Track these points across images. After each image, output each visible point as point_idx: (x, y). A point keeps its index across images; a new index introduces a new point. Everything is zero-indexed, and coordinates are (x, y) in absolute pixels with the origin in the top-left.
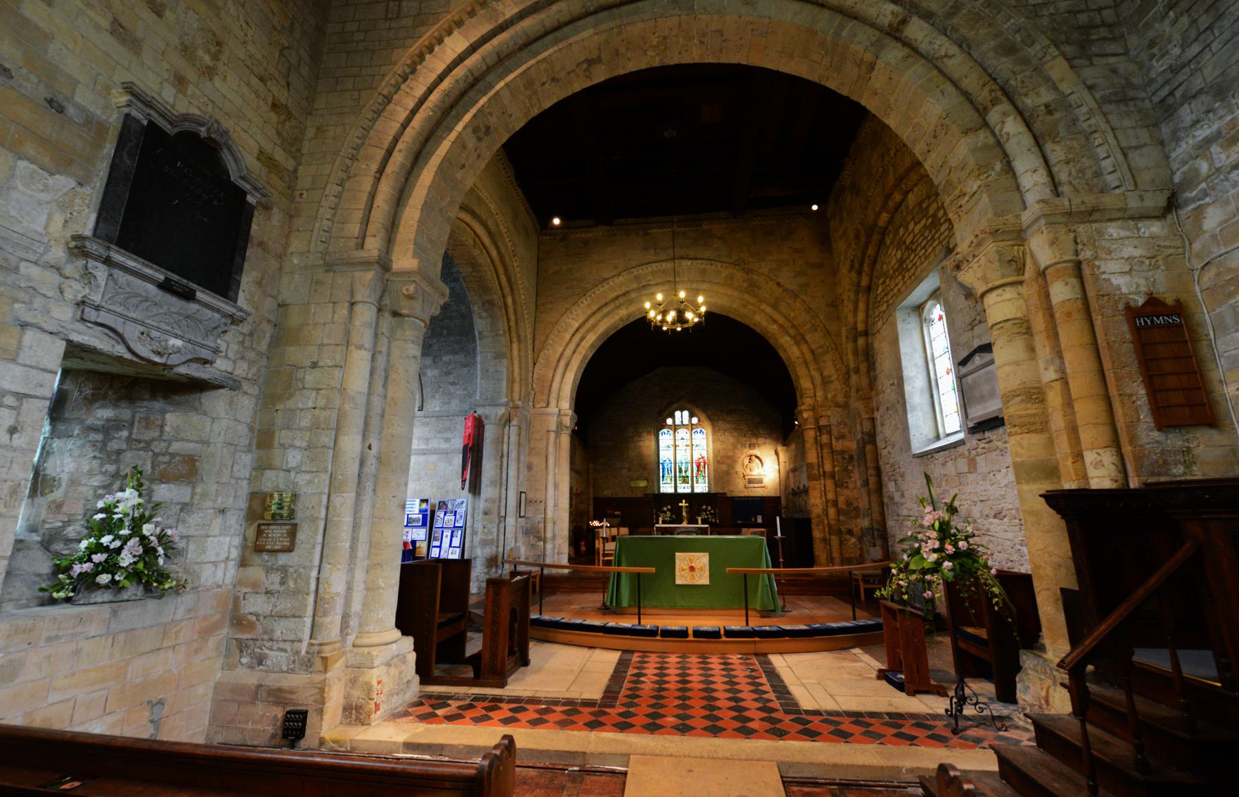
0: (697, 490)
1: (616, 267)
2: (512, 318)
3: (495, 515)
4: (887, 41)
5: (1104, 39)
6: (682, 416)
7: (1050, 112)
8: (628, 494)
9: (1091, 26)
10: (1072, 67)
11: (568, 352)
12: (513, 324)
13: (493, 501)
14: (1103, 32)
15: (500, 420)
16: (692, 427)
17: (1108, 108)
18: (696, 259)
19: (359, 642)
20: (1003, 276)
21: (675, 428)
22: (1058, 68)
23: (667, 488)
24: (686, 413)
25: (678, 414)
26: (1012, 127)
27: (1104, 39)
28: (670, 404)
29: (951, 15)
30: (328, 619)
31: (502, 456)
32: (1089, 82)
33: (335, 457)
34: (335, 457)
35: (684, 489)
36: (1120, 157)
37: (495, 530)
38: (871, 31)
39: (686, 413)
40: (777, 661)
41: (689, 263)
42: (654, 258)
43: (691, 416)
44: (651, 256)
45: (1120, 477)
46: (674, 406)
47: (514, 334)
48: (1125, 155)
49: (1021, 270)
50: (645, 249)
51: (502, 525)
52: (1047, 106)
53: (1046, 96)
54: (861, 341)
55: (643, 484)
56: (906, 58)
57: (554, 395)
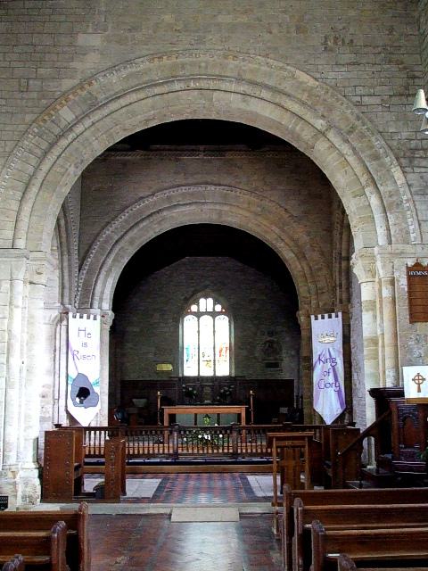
0: (218, 374)
1: (150, 188)
2: (64, 235)
3: (50, 399)
4: (320, 136)
5: (421, 157)
6: (206, 304)
7: (390, 196)
8: (155, 378)
9: (414, 150)
10: (404, 172)
11: (110, 261)
12: (64, 240)
13: (48, 386)
14: (421, 152)
15: (53, 321)
16: (214, 314)
17: (416, 198)
18: (220, 185)
19: (24, 466)
20: (367, 277)
21: (198, 315)
22: (397, 173)
23: (190, 370)
24: (210, 301)
25: (202, 301)
26: (374, 201)
27: (421, 157)
28: (194, 293)
29: (350, 132)
30: (11, 454)
31: (55, 351)
32: (409, 183)
33: (8, 369)
34: (8, 369)
35: (207, 372)
36: (417, 225)
37: (51, 410)
38: (312, 129)
39: (210, 301)
40: (251, 479)
41: (213, 188)
42: (184, 182)
43: (214, 304)
44: (180, 179)
45: (395, 382)
46: (199, 294)
47: (65, 248)
48: (420, 225)
49: (374, 276)
50: (177, 173)
51: (56, 406)
52: (390, 192)
53: (390, 188)
54: (344, 264)
55: (169, 367)
56: (329, 148)
57: (97, 298)
